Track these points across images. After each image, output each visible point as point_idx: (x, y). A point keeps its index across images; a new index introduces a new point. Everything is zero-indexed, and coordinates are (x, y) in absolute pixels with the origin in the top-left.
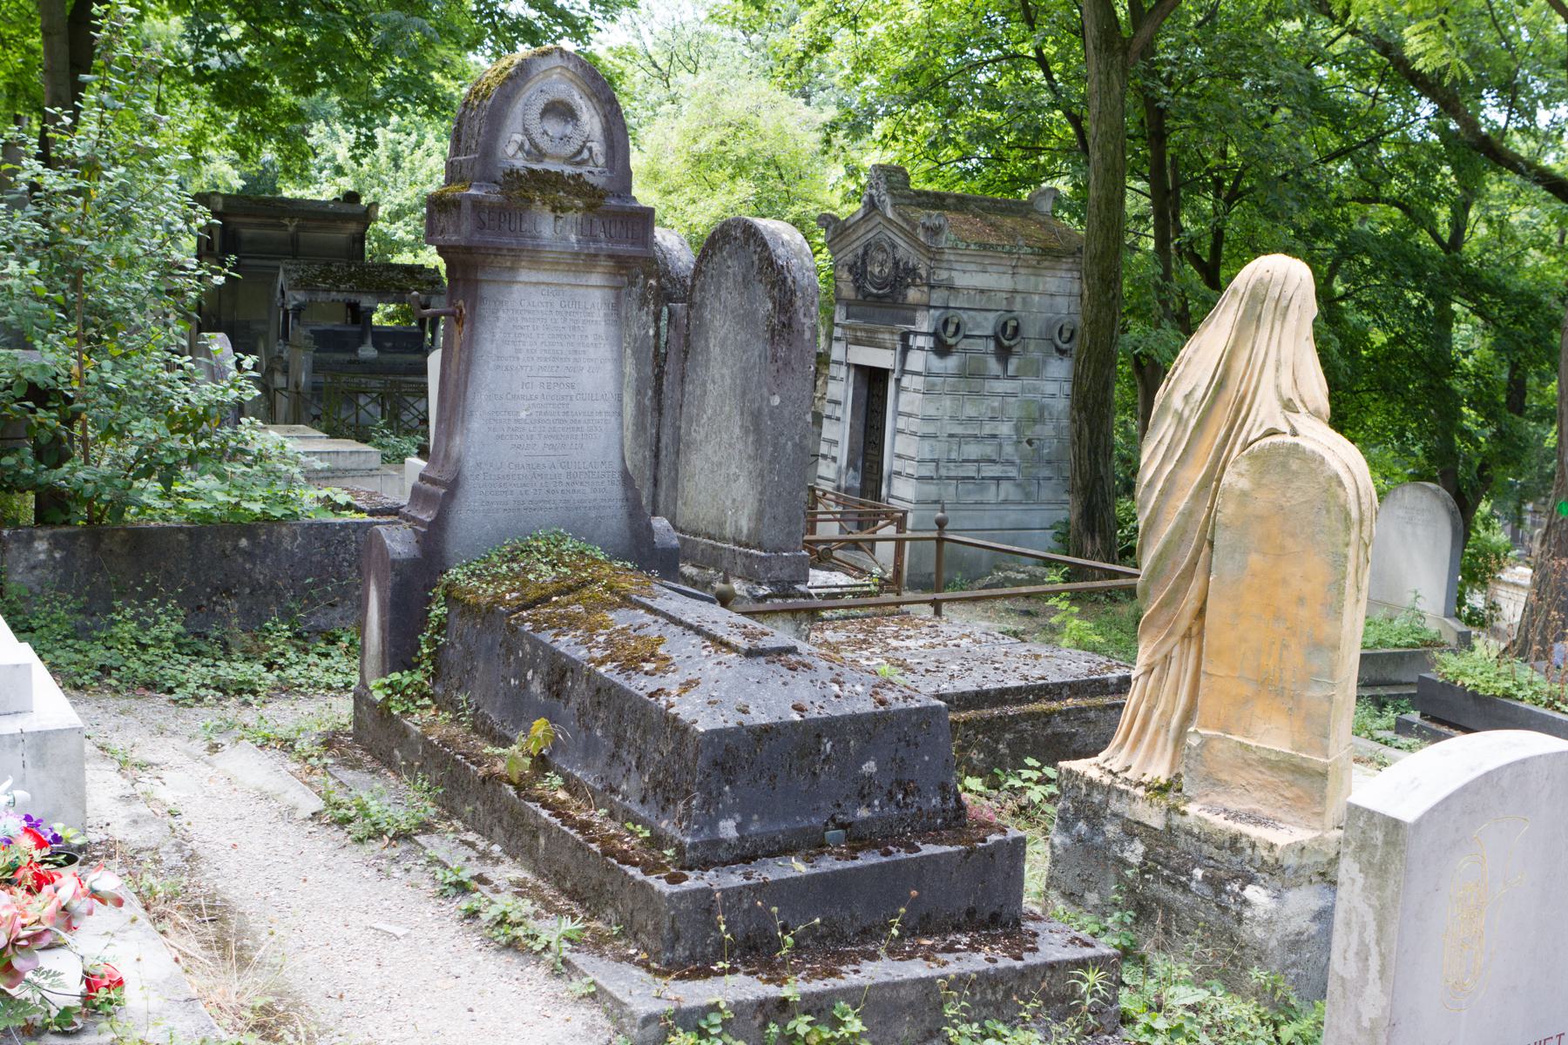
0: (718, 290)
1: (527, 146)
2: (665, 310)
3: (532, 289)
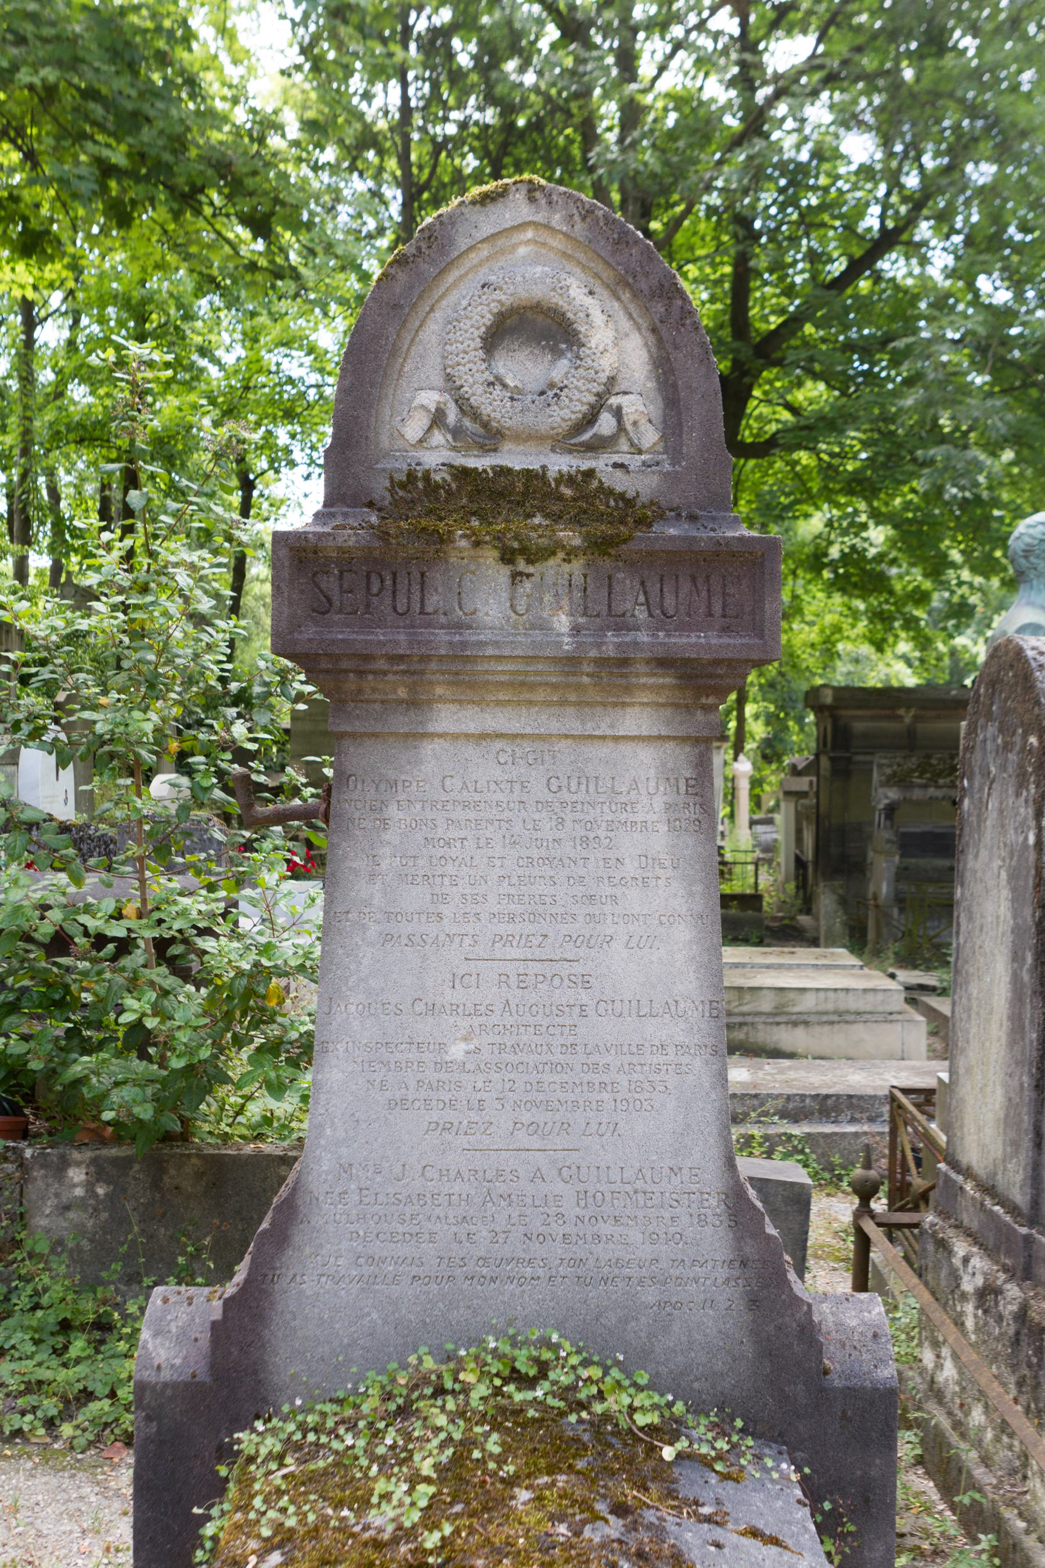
1: (452, 416)
3: (470, 751)
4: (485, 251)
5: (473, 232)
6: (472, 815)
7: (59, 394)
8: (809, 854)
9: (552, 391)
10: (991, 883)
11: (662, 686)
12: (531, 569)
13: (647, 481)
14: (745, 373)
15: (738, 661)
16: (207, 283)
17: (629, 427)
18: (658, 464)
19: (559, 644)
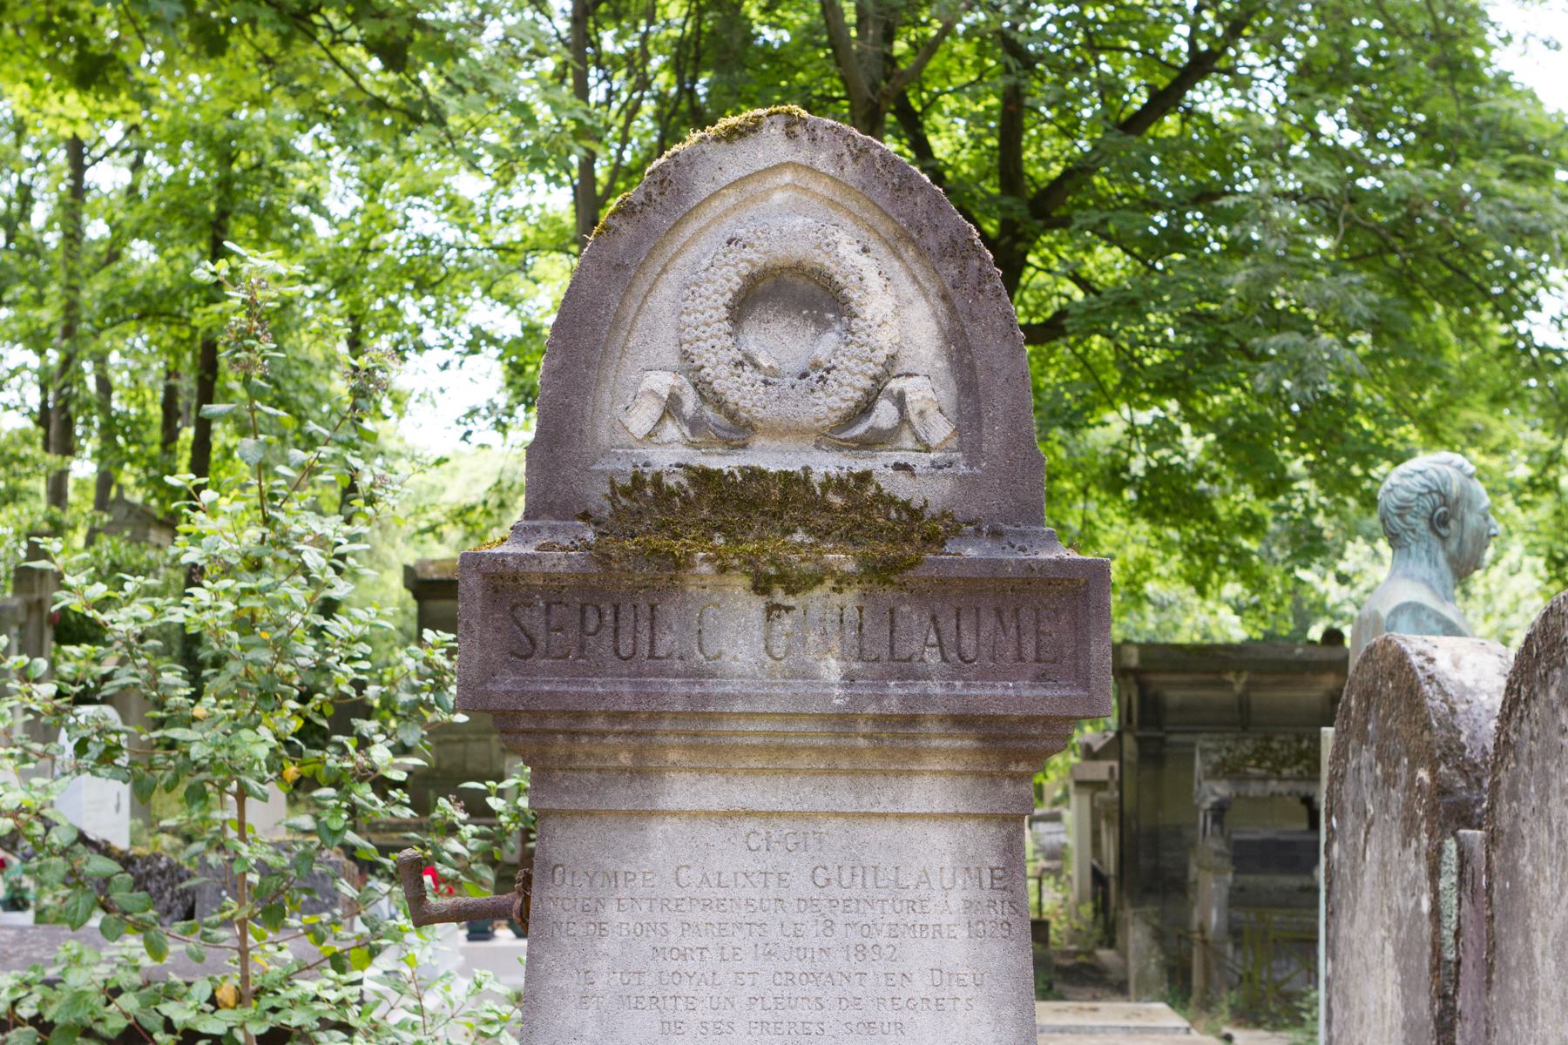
0: (1545, 798)
1: (690, 404)
2: (1451, 845)
3: (712, 833)
4: (731, 198)
5: (717, 174)
6: (714, 917)
7: (114, 256)
8: (1110, 867)
9: (817, 373)
10: (1373, 959)
11: (961, 750)
12: (791, 601)
13: (938, 486)
14: (1018, 238)
15: (1056, 718)
16: (314, 113)
17: (914, 418)
18: (950, 464)
19: (827, 698)
